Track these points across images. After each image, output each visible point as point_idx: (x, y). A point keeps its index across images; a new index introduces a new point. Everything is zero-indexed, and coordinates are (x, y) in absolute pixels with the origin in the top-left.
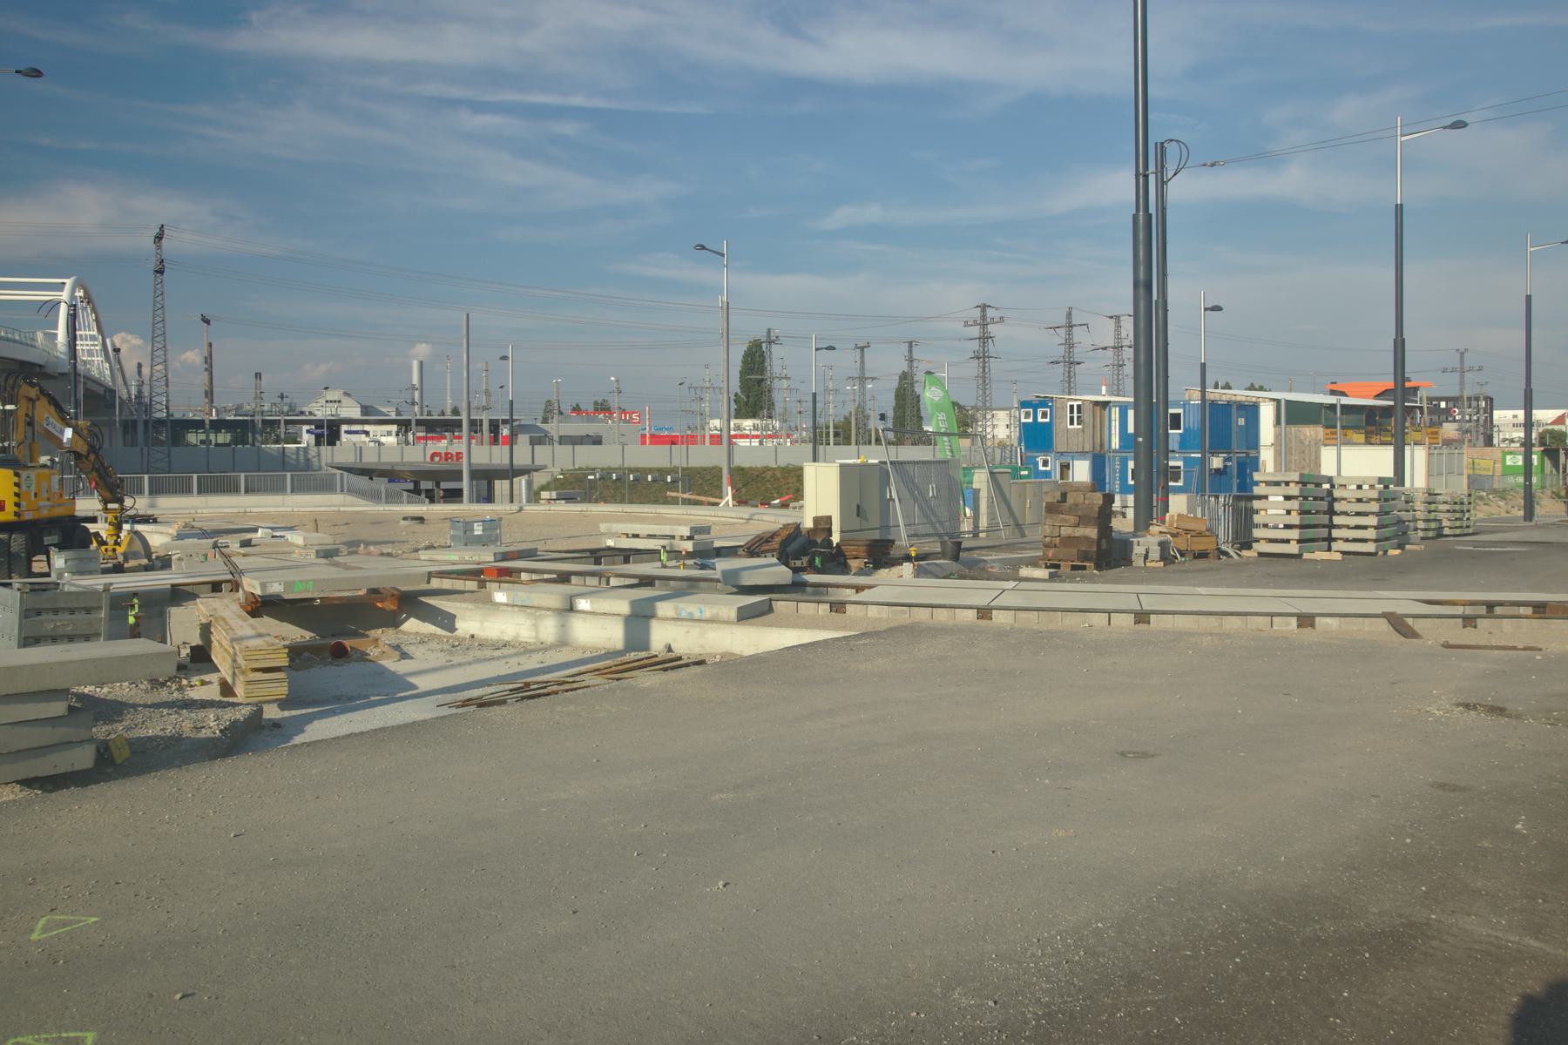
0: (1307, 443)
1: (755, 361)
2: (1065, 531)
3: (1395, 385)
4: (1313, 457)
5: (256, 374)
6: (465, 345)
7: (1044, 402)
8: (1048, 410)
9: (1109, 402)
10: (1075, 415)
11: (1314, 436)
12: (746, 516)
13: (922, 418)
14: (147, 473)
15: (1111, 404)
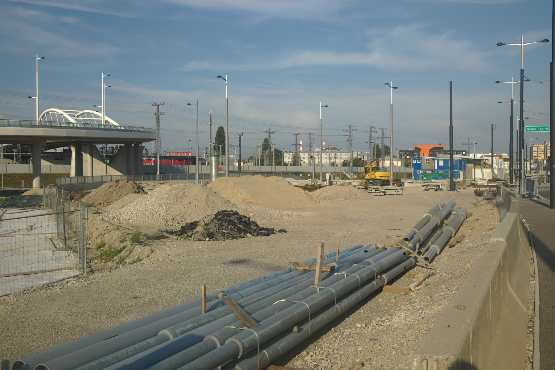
0: (469, 168)
3: (450, 149)
4: (471, 171)
10: (427, 161)
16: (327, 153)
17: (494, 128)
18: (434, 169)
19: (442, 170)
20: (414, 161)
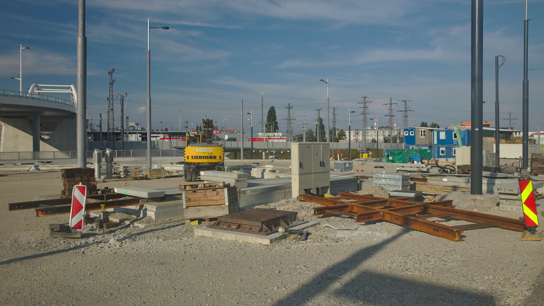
0: (489, 143)
1: (272, 114)
2: (539, 166)
4: (491, 147)
5: (127, 117)
6: (242, 109)
7: (412, 130)
8: (414, 132)
9: (434, 129)
10: (423, 133)
11: (491, 141)
12: (361, 163)
13: (325, 133)
14: (131, 149)
15: (434, 130)
16: (375, 131)
17: (500, 64)
18: (432, 143)
19: (443, 145)
20: (406, 133)
